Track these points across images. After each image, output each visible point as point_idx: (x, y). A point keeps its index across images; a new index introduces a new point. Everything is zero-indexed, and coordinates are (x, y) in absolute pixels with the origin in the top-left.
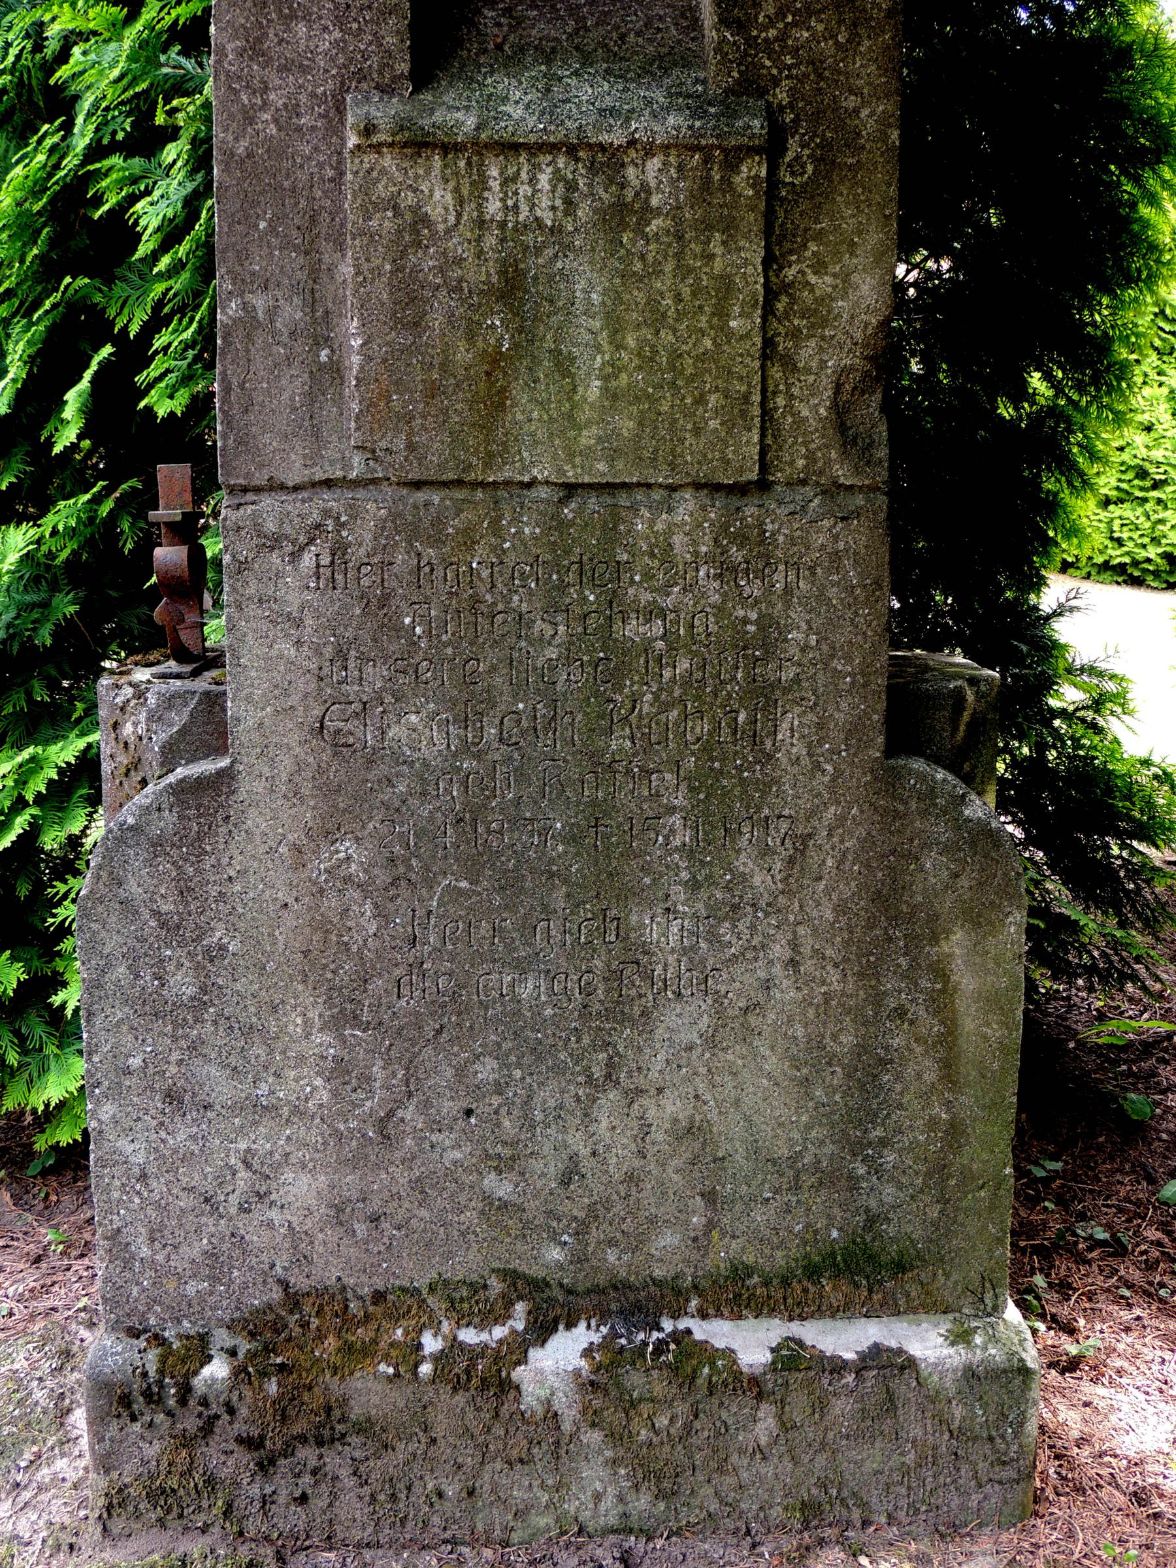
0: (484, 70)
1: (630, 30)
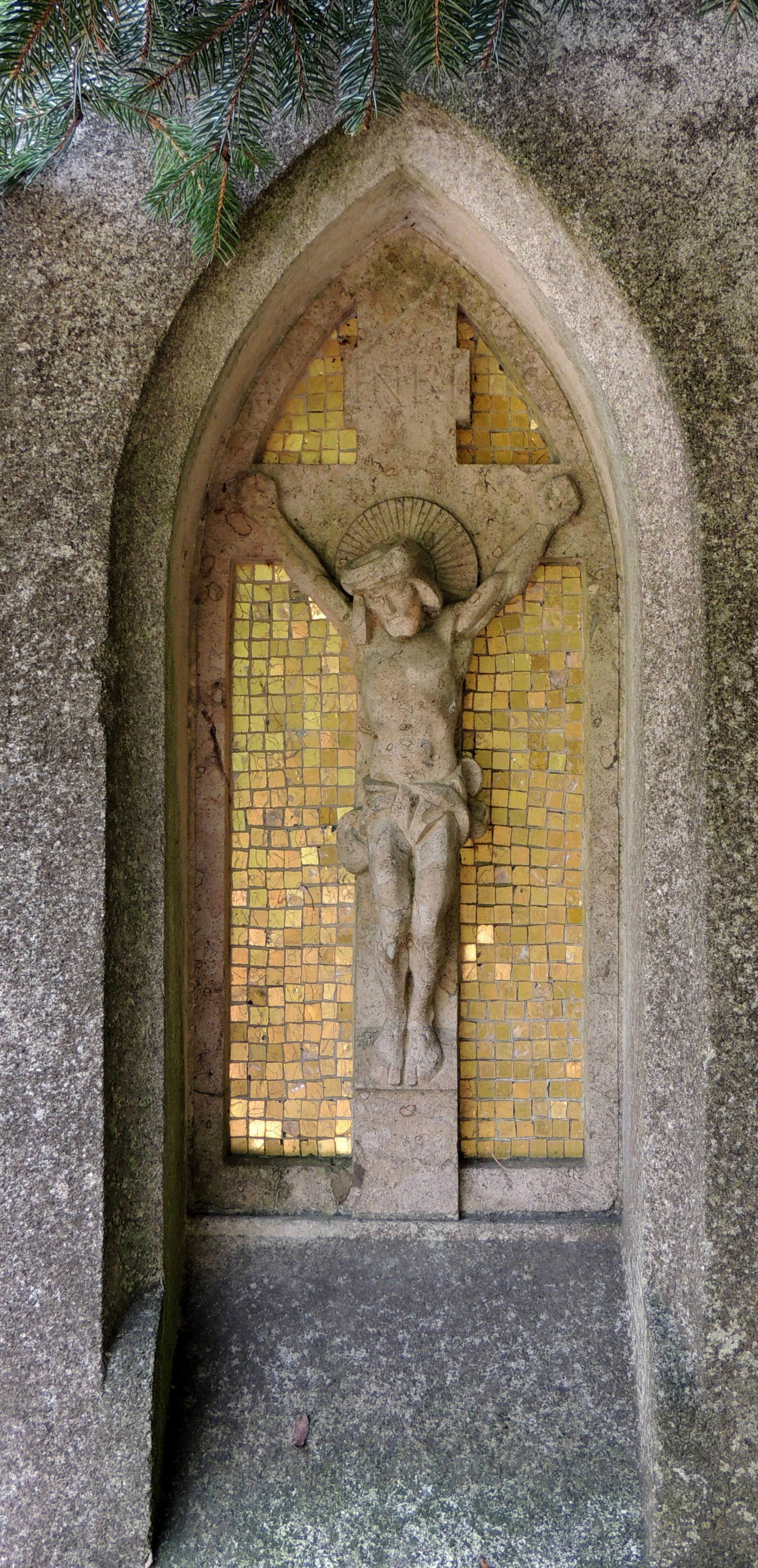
0: (275, 1502)
1: (516, 1394)
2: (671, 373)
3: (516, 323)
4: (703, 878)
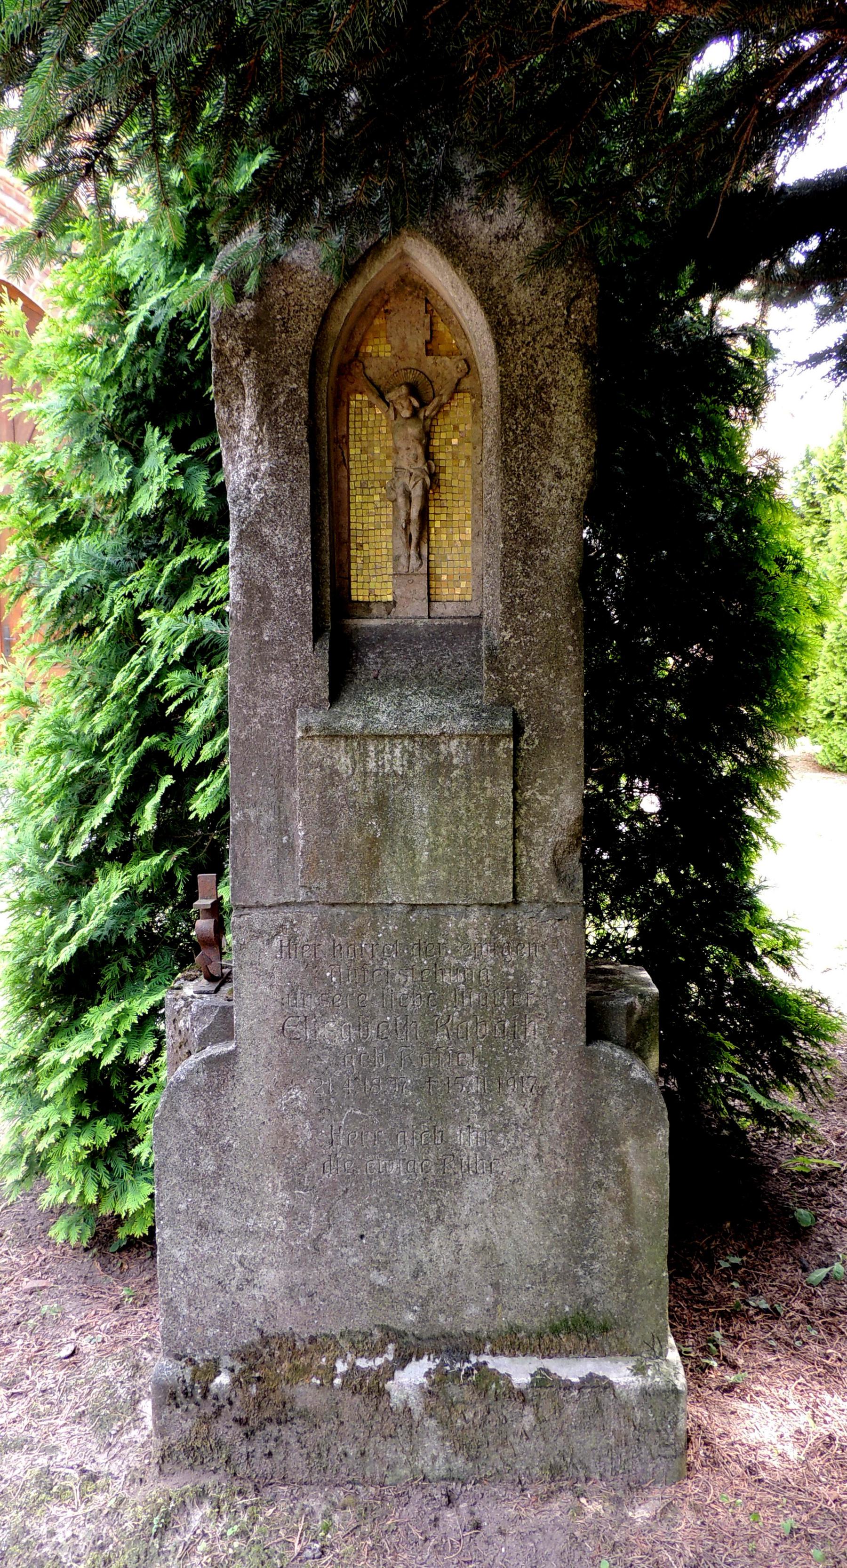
2: (490, 323)
3: (446, 304)
4: (500, 491)
